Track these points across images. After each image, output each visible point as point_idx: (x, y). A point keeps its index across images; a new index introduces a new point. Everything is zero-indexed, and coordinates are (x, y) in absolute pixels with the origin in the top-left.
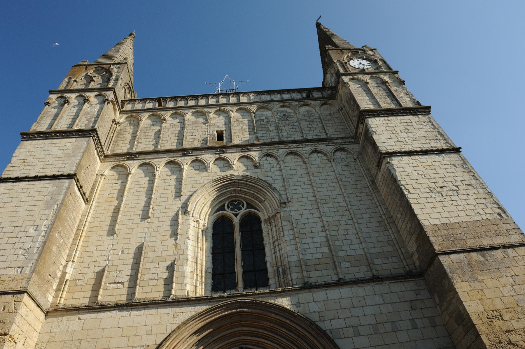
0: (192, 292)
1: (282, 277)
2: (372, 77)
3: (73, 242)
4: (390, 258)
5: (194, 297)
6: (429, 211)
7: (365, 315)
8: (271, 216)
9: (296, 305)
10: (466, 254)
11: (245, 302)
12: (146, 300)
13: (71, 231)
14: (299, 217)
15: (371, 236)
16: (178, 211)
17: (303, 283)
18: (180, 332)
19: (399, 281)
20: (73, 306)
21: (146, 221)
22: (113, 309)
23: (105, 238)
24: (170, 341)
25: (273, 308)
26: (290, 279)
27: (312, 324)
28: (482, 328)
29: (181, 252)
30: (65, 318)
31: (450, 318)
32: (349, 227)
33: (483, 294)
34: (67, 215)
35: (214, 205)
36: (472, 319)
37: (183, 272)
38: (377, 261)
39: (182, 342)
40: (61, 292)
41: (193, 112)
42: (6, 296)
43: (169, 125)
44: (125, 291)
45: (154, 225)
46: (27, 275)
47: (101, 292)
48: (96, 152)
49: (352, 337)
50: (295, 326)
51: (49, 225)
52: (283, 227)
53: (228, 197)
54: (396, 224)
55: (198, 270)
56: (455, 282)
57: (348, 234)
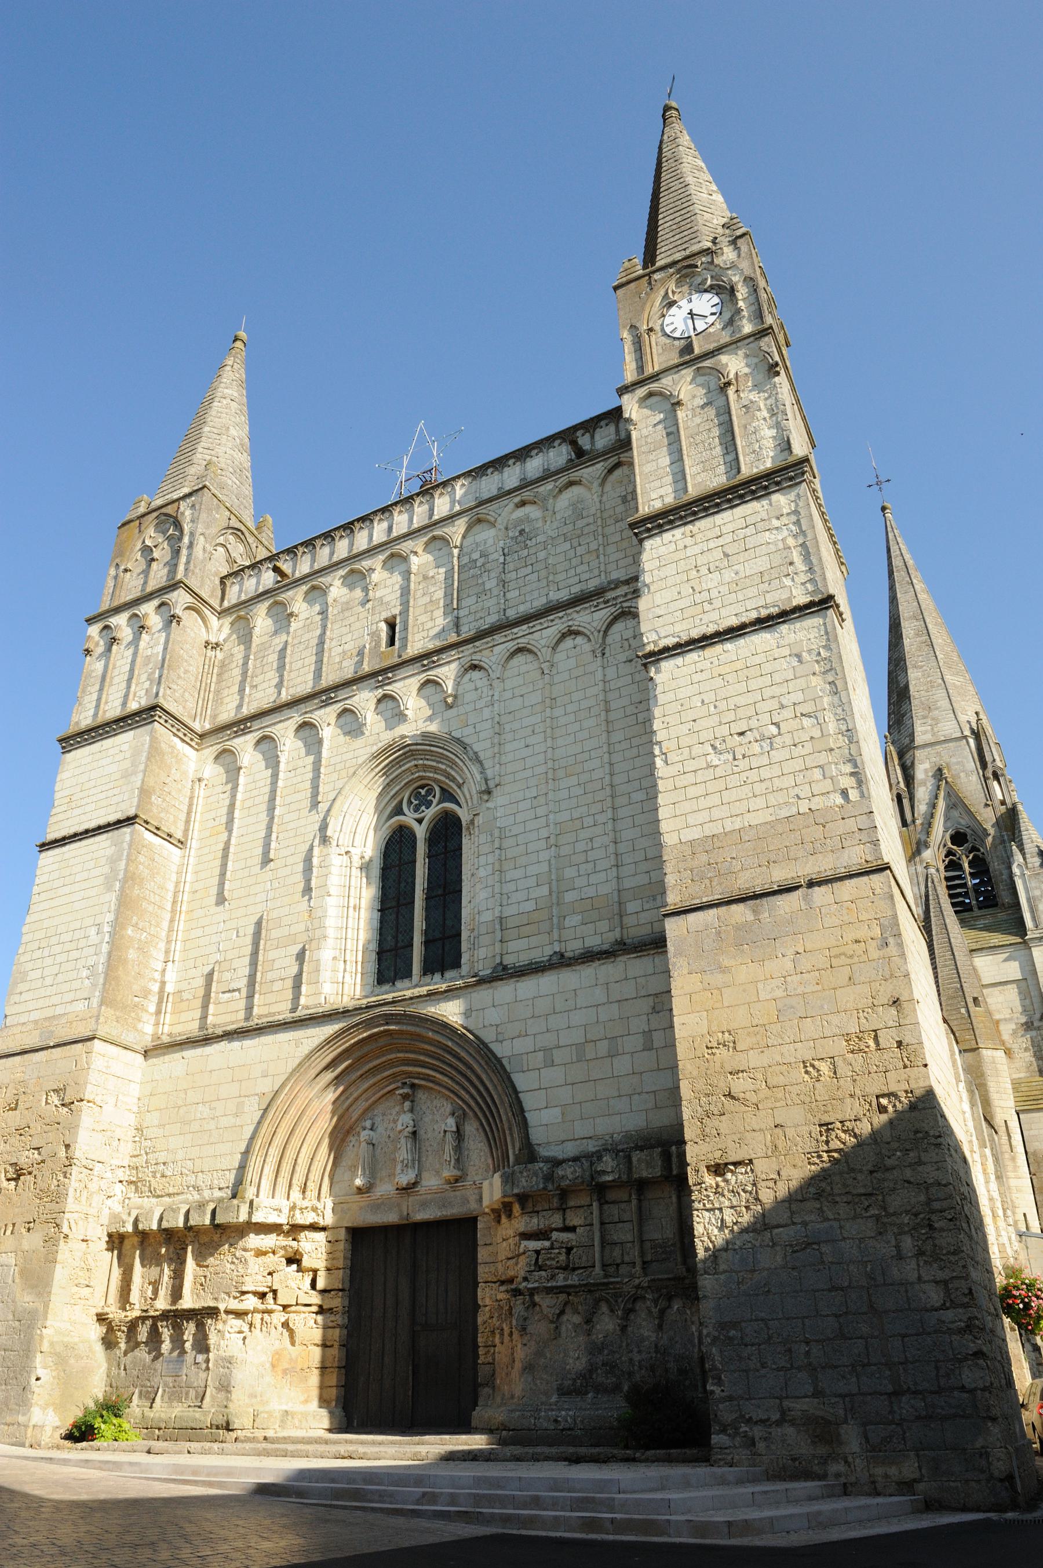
2: (701, 371)
10: (723, 910)
11: (392, 1015)
21: (268, 867)
28: (689, 1066)
30: (167, 1058)
35: (380, 808)
41: (342, 576)
43: (301, 624)
48: (177, 740)
53: (406, 784)
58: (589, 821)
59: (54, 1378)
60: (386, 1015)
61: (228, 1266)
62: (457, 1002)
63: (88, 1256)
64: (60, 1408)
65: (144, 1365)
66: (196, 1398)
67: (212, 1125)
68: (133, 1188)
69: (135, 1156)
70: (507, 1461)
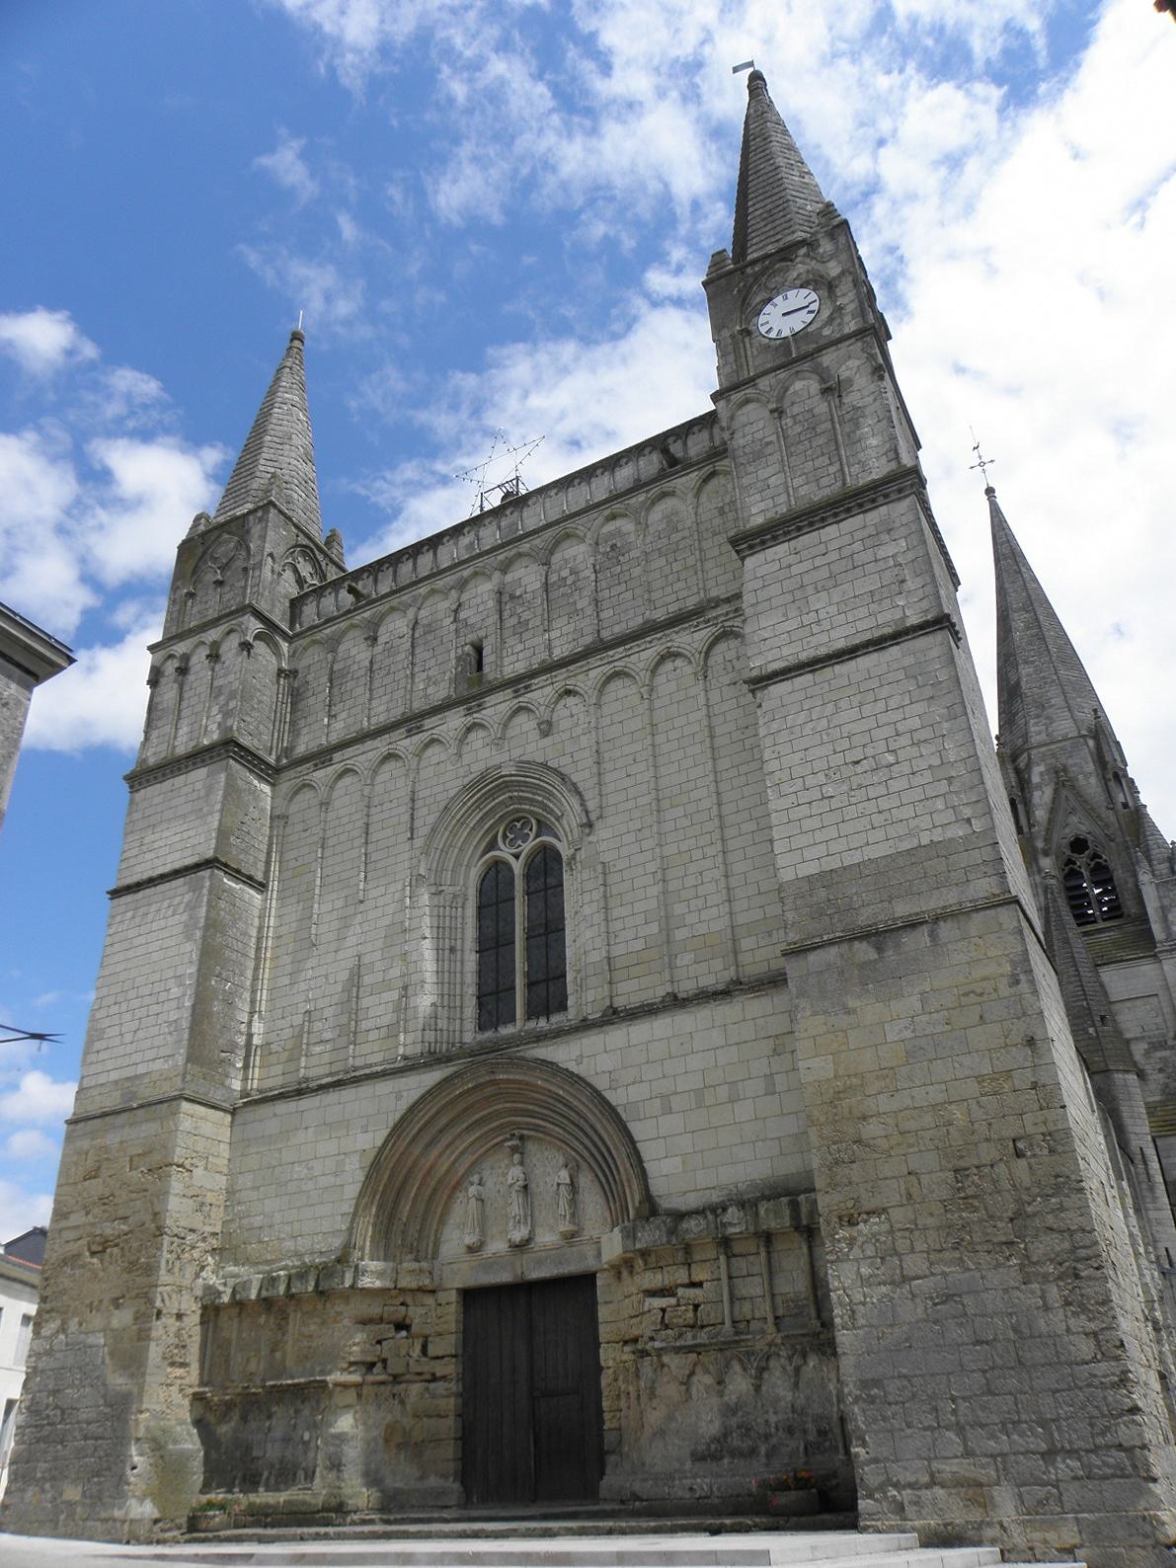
27: (598, 1094)
59: (151, 1465)
67: (310, 1185)
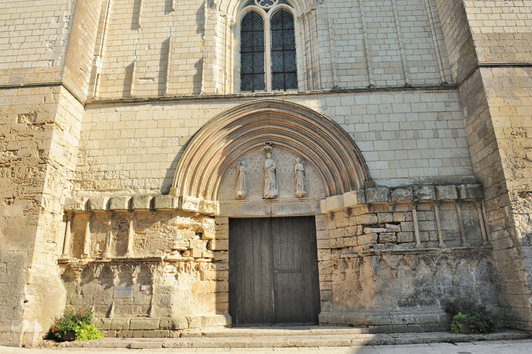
0: (221, 90)
1: (311, 80)
3: (97, 35)
4: (427, 68)
5: (223, 94)
6: (483, 17)
7: (389, 122)
8: (305, 13)
9: (322, 108)
10: (511, 69)
11: (273, 102)
12: (177, 96)
13: (93, 23)
14: (336, 16)
15: (412, 42)
16: (204, 4)
17: (332, 87)
18: (211, 126)
19: (431, 91)
20: (108, 99)
21: (170, 14)
22: (146, 103)
23: (129, 31)
24: (202, 133)
25: (301, 109)
26: (319, 82)
27: (336, 126)
28: (502, 142)
29: (208, 49)
30: (103, 110)
31: (473, 131)
32: (390, 30)
33: (515, 111)
34: (87, 5)
36: (496, 133)
37: (211, 69)
38: (412, 70)
39: (213, 135)
40: (95, 86)
42: (44, 88)
44: (156, 87)
45: (179, 18)
46: (59, 68)
47: (133, 86)
49: (373, 141)
50: (319, 127)
51: (70, 16)
52: (318, 26)
54: (443, 30)
55: (227, 69)
56: (490, 96)
57: (387, 38)
58: (384, 25)
59: (37, 301)
60: (269, 102)
61: (161, 234)
62: (316, 101)
63: (54, 223)
64: (42, 320)
65: (98, 291)
66: (143, 311)
67: (143, 152)
68: (79, 185)
69: (80, 166)
70: (407, 344)
